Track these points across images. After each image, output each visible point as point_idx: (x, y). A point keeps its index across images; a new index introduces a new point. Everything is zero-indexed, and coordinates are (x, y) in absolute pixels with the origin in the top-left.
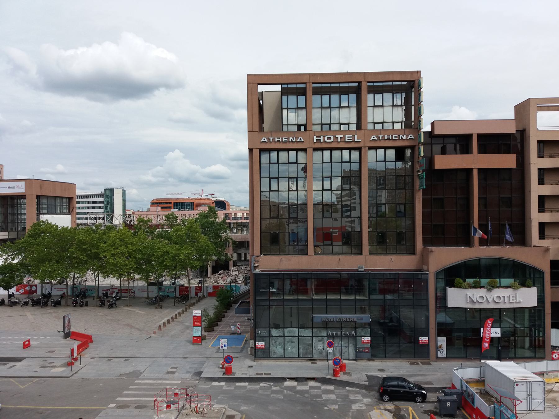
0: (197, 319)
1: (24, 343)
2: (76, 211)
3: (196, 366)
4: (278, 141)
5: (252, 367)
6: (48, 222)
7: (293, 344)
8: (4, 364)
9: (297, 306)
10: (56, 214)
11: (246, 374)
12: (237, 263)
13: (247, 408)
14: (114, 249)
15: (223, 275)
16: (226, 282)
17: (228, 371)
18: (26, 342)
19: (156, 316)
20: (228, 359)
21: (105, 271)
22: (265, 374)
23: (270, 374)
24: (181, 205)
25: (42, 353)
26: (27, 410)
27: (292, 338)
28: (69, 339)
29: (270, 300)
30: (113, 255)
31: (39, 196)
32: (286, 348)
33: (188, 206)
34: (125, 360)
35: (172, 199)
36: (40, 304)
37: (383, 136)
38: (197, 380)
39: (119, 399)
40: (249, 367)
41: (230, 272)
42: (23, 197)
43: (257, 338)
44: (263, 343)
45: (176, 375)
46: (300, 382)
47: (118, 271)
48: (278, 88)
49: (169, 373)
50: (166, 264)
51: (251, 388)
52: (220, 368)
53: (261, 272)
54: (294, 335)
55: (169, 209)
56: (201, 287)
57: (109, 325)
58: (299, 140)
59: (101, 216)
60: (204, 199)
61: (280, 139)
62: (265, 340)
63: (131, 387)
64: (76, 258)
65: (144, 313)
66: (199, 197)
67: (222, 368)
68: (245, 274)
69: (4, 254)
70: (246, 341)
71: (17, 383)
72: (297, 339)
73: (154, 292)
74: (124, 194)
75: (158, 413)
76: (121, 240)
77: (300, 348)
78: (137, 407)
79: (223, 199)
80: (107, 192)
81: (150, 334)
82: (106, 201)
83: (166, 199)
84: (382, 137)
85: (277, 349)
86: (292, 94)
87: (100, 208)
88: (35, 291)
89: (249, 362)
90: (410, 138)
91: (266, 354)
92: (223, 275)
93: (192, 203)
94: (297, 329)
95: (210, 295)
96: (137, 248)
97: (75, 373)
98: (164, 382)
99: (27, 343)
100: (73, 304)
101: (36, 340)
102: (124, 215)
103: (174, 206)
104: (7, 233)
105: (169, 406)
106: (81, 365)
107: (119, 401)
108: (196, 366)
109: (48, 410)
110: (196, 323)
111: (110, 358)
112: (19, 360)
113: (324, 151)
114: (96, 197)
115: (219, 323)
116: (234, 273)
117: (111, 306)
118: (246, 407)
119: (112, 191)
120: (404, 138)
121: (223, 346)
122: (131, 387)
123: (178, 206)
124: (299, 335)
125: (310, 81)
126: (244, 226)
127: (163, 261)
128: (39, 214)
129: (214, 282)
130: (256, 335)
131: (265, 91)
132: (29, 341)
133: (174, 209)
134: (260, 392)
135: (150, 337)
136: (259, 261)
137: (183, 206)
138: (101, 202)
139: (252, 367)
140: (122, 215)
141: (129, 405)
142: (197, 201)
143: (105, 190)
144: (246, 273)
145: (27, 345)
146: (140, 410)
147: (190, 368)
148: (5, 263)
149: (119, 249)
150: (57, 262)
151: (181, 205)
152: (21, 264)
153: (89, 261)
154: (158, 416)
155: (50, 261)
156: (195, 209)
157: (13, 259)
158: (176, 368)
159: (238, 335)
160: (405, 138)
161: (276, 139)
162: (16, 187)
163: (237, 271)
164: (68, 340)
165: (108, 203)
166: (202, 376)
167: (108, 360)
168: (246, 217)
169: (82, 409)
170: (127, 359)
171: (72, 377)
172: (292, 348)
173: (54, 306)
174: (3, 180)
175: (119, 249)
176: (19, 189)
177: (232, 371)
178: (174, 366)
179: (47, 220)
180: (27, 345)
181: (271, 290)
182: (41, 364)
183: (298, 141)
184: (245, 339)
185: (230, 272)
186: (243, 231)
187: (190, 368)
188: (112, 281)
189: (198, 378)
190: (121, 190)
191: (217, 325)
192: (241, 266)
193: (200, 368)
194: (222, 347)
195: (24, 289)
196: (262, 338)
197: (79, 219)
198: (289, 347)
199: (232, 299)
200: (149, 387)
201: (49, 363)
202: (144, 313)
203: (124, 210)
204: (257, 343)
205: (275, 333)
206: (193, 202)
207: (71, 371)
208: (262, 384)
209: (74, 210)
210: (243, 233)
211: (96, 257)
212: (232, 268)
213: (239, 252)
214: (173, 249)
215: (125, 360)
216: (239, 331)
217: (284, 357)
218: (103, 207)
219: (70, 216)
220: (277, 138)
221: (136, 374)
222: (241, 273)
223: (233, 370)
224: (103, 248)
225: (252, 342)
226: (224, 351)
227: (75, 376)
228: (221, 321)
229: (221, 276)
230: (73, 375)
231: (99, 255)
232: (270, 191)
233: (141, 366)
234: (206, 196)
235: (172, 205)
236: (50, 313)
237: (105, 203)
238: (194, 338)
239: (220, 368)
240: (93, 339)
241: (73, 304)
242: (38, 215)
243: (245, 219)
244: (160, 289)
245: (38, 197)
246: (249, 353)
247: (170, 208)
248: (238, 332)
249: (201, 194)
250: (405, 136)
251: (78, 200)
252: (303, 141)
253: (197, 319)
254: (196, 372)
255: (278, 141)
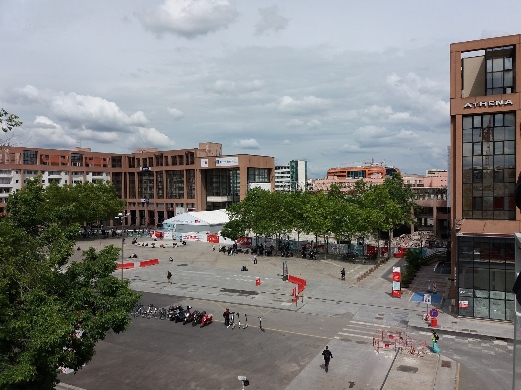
0: (396, 275)
1: (257, 281)
2: (274, 180)
3: (400, 315)
4: (483, 105)
5: (456, 323)
6: (260, 189)
7: (499, 307)
8: (247, 296)
9: (504, 271)
10: (255, 182)
11: (452, 328)
12: (418, 228)
13: (460, 358)
14: (315, 210)
15: (405, 238)
16: (408, 245)
17: (434, 323)
18: (258, 280)
19: (351, 270)
20: (434, 313)
21: (307, 227)
22: (471, 331)
23: (476, 332)
24: (354, 173)
25: (271, 290)
26: (273, 332)
27: (499, 301)
28: (287, 281)
29: (474, 263)
30: (315, 215)
31: (249, 168)
32: (492, 310)
33: (361, 174)
34: (337, 303)
35: (346, 168)
36: (257, 253)
37: (478, 103)
38: (405, 327)
39: (340, 333)
40: (453, 322)
41: (411, 236)
42: (237, 169)
43: (460, 297)
44: (467, 303)
45: (384, 321)
46: (510, 342)
47: (317, 229)
48: (482, 53)
49: (377, 318)
50: (359, 225)
51: (460, 341)
52: (424, 320)
53: (463, 235)
54: (501, 298)
55: (343, 178)
56: (387, 247)
57: (314, 274)
58: (507, 102)
59: (287, 184)
60: (376, 167)
61: (486, 104)
62: (469, 300)
63: (347, 325)
64: (285, 217)
65: (340, 266)
66: (369, 165)
67: (427, 320)
68: (428, 238)
69: (230, 213)
70: (444, 300)
71: (259, 311)
72: (504, 303)
73: (343, 249)
74: (306, 166)
75: (378, 349)
76: (320, 203)
77: (507, 311)
78: (358, 342)
79: (392, 167)
80: (293, 164)
81: (352, 284)
82: (291, 171)
83: (341, 169)
84: (477, 104)
85: (481, 309)
86: (498, 57)
87: (287, 177)
88: (251, 243)
89: (451, 318)
90: (507, 104)
91: (470, 313)
92: (405, 238)
93: (364, 172)
94: (504, 293)
95: (396, 255)
96: (332, 210)
97: (300, 308)
98: (375, 325)
99: (258, 281)
100: (282, 254)
101: (263, 280)
102: (307, 184)
103: (348, 174)
104: (226, 197)
105: (387, 345)
106: (302, 302)
107: (340, 335)
108: (400, 315)
109: (288, 333)
110: (395, 278)
111: (324, 301)
112: (256, 294)
113: (474, 117)
114: (284, 169)
115: (412, 281)
116: (416, 237)
117: (312, 258)
118: (459, 357)
119: (296, 163)
120: (500, 104)
121: (427, 301)
122: (347, 325)
123: (351, 175)
124: (506, 298)
125: (520, 42)
126: (426, 192)
127: (357, 222)
128: (248, 183)
129: (396, 244)
130: (459, 294)
131: (465, 58)
132: (259, 279)
133: (348, 177)
134: (470, 346)
135: (352, 286)
136: (461, 225)
137: (356, 174)
138: (288, 173)
139: (456, 323)
140: (304, 183)
141: (351, 339)
142: (369, 169)
143: (291, 162)
144: (428, 237)
145: (258, 283)
146: (361, 345)
147: (395, 316)
148: (231, 219)
149: (318, 211)
150: (270, 220)
151: (354, 173)
152: (243, 221)
153: (294, 219)
154: (378, 352)
155: (265, 219)
156: (367, 176)
157: (236, 217)
158: (383, 315)
159: (434, 293)
160: (502, 104)
161: (481, 104)
162: (232, 161)
163: (419, 236)
164: (286, 282)
165: (293, 172)
166: (408, 324)
167: (323, 301)
168: (420, 184)
169: (314, 337)
170: (338, 302)
171: (298, 311)
172: (498, 310)
173: (268, 255)
174: (222, 156)
175: (318, 211)
176: (234, 162)
177: (438, 324)
178: (381, 313)
179: (260, 187)
180: (258, 283)
181: (475, 253)
182: (272, 298)
183: (506, 103)
184: (442, 298)
185: (411, 236)
186: (424, 197)
187: (395, 316)
188: (310, 237)
189: (405, 326)
190: (304, 162)
191: (411, 283)
192: (422, 231)
193: (405, 318)
194: (426, 301)
195: (243, 241)
196: (465, 298)
197: (277, 186)
198: (495, 309)
199: (420, 261)
200: (363, 327)
201: (278, 298)
202: (340, 266)
203: (306, 179)
204: (460, 302)
205: (479, 294)
206: (366, 171)
207: (297, 306)
208: (469, 339)
209: (273, 179)
210: (425, 199)
211: (300, 217)
212: (413, 232)
213: (420, 217)
214: (364, 212)
215: (337, 303)
216: (435, 290)
217: (489, 318)
218: (289, 176)
219: (270, 184)
220: (482, 103)
221: (349, 316)
222: (423, 237)
223: (438, 323)
224: (305, 210)
225: (453, 301)
226: (428, 306)
227: (300, 310)
228: (413, 279)
229: (403, 239)
230: (298, 309)
231: (302, 215)
232: (473, 155)
233: (353, 310)
234: (376, 164)
235: (346, 174)
236: (266, 260)
237: (291, 173)
238: (394, 292)
239: (424, 320)
240: (306, 283)
241: (282, 254)
242: (248, 183)
243: (418, 186)
244: (349, 247)
245: (248, 168)
246: (450, 310)
247: (344, 176)
248: (434, 291)
249: (372, 162)
250: (502, 101)
251: (276, 171)
252: (512, 103)
253: (396, 275)
254: (402, 321)
255: (483, 105)
